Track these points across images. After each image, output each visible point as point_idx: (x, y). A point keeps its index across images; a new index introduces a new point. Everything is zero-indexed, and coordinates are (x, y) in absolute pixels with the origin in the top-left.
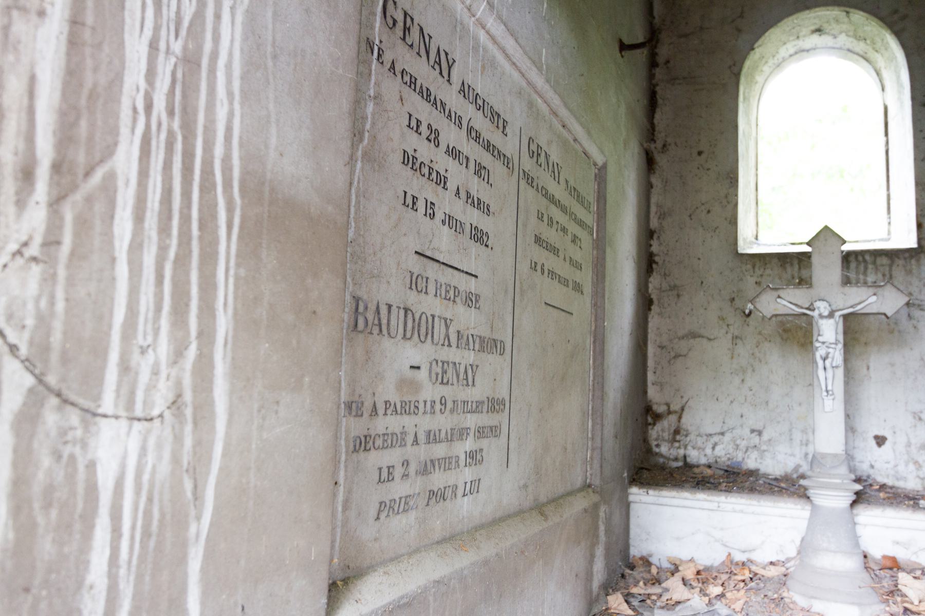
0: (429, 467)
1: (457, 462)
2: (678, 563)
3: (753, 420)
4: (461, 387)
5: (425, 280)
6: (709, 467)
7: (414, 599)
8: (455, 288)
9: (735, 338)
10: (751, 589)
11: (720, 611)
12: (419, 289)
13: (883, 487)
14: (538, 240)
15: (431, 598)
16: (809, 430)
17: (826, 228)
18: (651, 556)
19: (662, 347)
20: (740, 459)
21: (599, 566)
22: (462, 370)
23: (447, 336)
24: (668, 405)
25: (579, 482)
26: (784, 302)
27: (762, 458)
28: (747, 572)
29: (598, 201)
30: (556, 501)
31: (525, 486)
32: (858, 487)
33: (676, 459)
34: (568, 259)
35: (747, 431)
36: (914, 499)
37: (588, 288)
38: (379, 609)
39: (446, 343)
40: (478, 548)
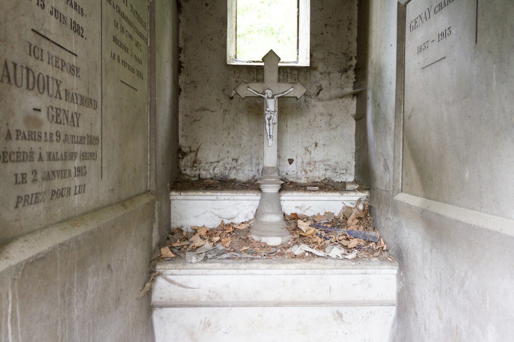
0: (51, 176)
1: (70, 173)
2: (197, 229)
3: (233, 154)
4: (70, 126)
5: (40, 51)
6: (212, 179)
7: (47, 254)
8: (62, 60)
9: (225, 111)
10: (233, 236)
11: (219, 248)
12: (37, 56)
13: (292, 183)
14: (115, 39)
15: (58, 254)
16: (260, 157)
17: (271, 51)
18: (182, 227)
19: (186, 116)
20: (227, 174)
21: (155, 234)
22: (70, 115)
23: (58, 92)
24: (190, 148)
25: (143, 189)
26: (250, 90)
27: (237, 173)
28: (231, 228)
29: (150, 23)
30: (131, 199)
31: (113, 190)
32: (282, 182)
33: (195, 176)
34: (133, 56)
35: (230, 160)
36: (305, 187)
37: (146, 76)
38: (22, 262)
39: (58, 96)
40: (86, 225)
